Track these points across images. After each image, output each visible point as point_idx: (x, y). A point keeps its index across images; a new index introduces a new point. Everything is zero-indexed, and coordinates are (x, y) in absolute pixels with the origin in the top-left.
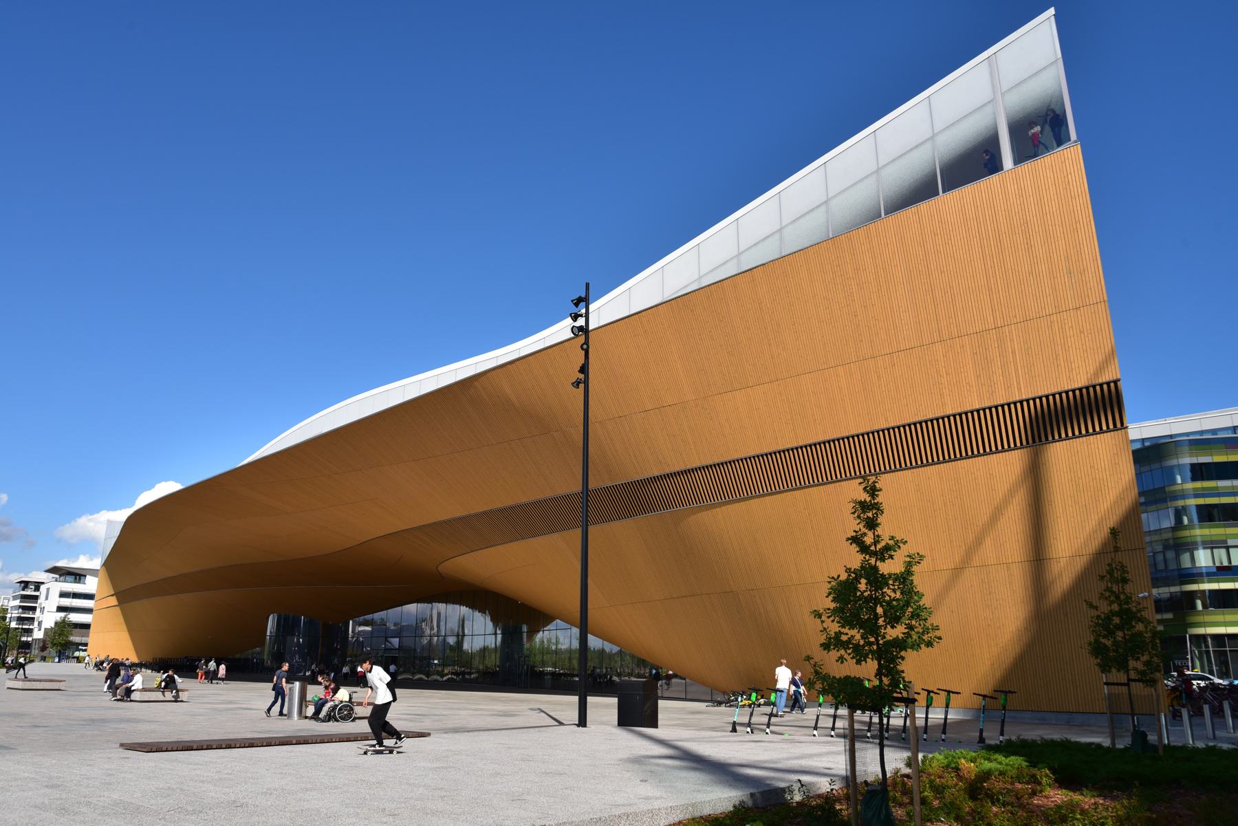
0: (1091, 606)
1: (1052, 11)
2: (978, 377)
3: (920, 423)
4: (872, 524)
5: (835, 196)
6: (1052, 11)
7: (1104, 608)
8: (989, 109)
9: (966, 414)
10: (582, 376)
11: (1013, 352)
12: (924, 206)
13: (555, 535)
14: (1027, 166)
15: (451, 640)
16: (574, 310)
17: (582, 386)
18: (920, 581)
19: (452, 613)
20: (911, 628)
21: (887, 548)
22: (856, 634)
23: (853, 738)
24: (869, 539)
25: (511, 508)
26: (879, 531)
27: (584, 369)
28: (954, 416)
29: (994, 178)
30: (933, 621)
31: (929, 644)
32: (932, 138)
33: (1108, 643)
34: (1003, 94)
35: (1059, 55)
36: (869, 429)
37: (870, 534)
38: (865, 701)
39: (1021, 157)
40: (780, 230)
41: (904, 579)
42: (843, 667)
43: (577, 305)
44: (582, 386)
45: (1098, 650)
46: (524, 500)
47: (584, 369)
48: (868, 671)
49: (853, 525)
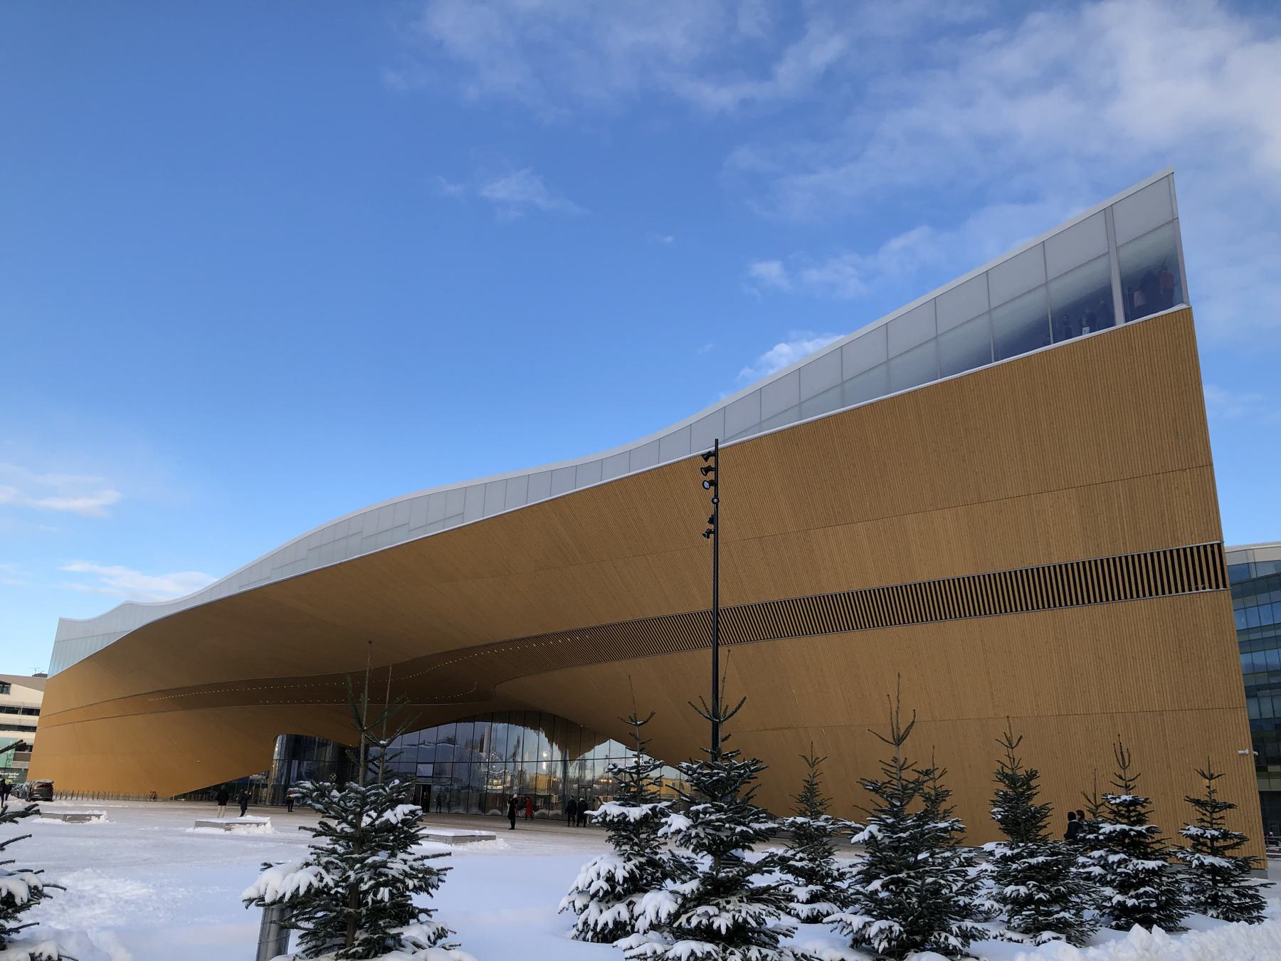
10: (712, 527)
16: (706, 465)
43: (706, 459)
44: (712, 536)
47: (713, 520)
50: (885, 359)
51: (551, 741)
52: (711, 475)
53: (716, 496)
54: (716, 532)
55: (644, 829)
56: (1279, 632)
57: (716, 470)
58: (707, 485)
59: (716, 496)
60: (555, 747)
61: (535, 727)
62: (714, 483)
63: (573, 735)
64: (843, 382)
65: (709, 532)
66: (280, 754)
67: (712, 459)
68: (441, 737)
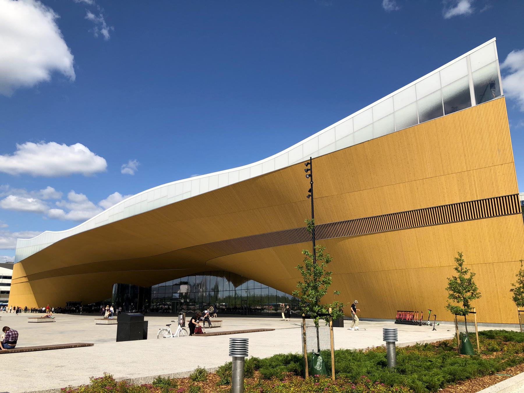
0: (513, 285)
1: (495, 39)
2: (460, 190)
3: (435, 208)
4: (461, 265)
5: (397, 111)
6: (495, 39)
7: (518, 285)
8: (466, 79)
9: (454, 205)
10: (310, 194)
11: (474, 181)
12: (437, 120)
13: (270, 249)
14: (482, 105)
15: (212, 293)
16: (307, 168)
17: (310, 197)
18: (475, 280)
19: (212, 280)
20: (473, 293)
21: (465, 272)
22: (457, 295)
23: (456, 322)
24: (460, 269)
25: (251, 237)
26: (463, 266)
27: (311, 191)
28: (449, 205)
29: (468, 109)
30: (478, 291)
31: (478, 298)
32: (440, 89)
33: (520, 297)
34: (472, 73)
35: (497, 58)
36: (413, 209)
37: (460, 267)
38: (462, 313)
39: (479, 101)
40: (373, 123)
41: (470, 280)
42: (454, 303)
43: (307, 165)
44: (310, 197)
45: (515, 299)
46: (257, 233)
47: (311, 191)
48: (461, 305)
49: (456, 265)
50: (415, 100)
51: (229, 281)
52: (309, 172)
53: (312, 181)
54: (312, 196)
55: (101, 307)
56: (1, 303)
57: (311, 170)
58: (308, 176)
59: (312, 181)
60: (231, 283)
61: (222, 276)
62: (311, 175)
63: (237, 279)
64: (354, 132)
65: (309, 196)
66: (115, 292)
67: (309, 165)
68: (174, 283)
